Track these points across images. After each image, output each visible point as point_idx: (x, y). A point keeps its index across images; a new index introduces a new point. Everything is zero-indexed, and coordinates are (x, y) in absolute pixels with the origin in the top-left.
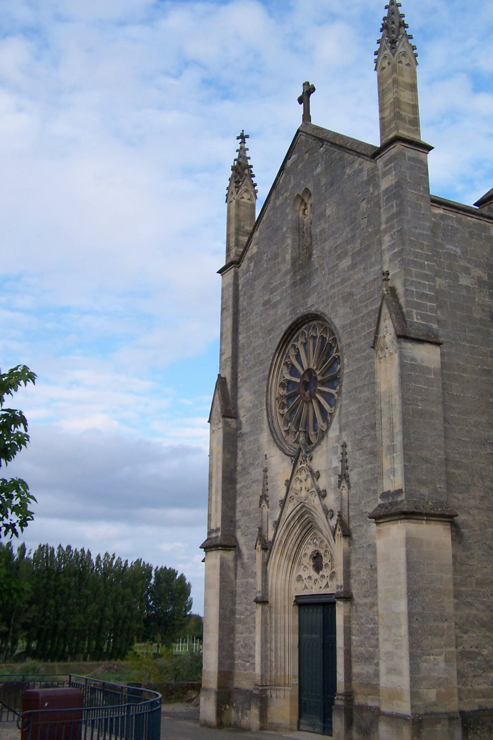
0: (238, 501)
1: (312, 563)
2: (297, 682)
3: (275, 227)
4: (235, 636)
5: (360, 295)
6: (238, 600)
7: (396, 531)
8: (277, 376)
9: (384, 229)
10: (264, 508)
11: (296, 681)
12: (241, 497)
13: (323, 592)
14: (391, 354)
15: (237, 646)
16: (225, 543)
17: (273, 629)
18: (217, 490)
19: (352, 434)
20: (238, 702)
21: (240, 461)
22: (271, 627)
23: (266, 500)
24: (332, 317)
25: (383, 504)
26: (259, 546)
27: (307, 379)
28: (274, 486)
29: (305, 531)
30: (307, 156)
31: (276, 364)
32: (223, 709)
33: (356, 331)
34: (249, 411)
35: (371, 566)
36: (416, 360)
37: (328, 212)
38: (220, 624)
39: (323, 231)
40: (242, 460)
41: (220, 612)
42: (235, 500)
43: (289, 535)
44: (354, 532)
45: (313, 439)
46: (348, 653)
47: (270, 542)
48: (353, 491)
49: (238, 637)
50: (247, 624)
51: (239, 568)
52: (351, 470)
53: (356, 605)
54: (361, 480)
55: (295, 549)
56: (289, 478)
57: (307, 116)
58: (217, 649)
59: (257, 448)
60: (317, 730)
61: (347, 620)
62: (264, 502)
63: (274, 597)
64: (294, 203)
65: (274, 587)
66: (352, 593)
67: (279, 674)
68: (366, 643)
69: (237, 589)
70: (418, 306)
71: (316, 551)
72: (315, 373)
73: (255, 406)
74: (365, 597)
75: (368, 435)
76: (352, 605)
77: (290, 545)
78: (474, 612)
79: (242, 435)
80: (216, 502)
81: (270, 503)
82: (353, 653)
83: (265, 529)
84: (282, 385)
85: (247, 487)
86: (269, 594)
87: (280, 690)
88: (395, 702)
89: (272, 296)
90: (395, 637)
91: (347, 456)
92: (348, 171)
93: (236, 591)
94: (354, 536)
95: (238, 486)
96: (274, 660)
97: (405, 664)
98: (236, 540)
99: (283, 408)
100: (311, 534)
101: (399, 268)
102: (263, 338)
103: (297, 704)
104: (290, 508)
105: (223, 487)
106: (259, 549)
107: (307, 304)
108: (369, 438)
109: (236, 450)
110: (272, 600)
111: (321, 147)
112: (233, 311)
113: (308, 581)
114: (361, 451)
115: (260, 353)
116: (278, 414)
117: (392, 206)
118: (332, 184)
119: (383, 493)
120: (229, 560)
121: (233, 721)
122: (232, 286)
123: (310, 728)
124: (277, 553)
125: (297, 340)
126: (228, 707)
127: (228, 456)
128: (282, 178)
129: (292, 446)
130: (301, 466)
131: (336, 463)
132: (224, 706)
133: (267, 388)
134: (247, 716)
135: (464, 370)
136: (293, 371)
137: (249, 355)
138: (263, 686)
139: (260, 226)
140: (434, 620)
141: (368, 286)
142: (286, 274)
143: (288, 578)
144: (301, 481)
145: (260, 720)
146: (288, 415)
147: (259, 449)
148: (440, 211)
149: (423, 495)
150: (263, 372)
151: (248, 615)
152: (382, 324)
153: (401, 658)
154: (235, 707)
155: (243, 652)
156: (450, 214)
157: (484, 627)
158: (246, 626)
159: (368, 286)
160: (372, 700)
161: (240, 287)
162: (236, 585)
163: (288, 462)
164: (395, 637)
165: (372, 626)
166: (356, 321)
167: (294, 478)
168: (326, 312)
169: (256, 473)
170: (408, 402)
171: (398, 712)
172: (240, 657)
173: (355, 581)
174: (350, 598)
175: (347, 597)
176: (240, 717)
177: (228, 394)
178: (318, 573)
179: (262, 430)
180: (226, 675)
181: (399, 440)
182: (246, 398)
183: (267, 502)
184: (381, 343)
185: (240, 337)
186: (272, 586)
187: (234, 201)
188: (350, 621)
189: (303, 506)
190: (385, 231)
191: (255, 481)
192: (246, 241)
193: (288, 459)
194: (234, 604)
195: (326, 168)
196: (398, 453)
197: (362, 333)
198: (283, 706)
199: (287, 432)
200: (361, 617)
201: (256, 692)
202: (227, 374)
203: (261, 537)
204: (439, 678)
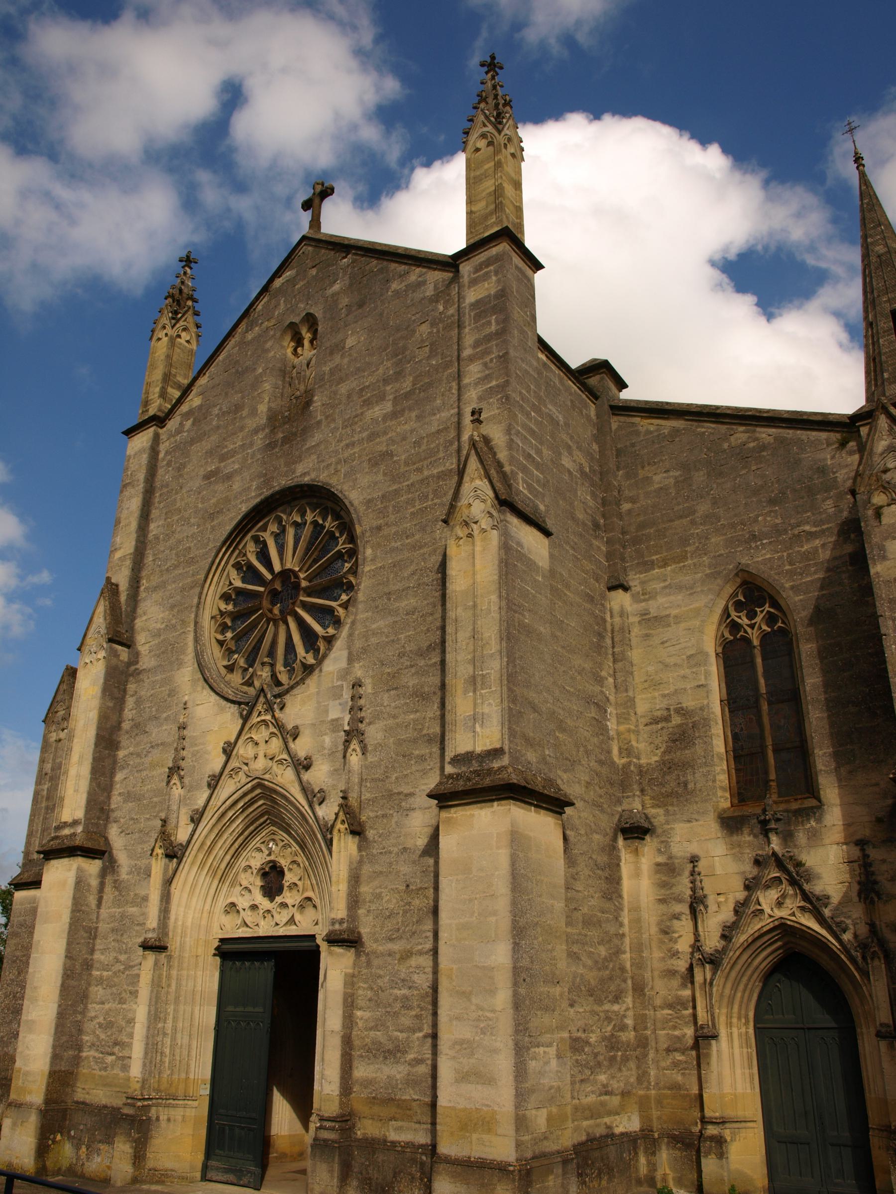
0: (119, 777)
1: (259, 882)
2: (208, 1092)
3: (240, 369)
4: (86, 1007)
5: (407, 455)
6: (99, 944)
7: (490, 821)
8: (218, 583)
9: (470, 356)
10: (174, 787)
11: (206, 1091)
12: (125, 771)
13: (281, 931)
14: (484, 531)
15: (89, 1026)
16: (89, 845)
17: (172, 997)
18: (81, 757)
19: (375, 664)
20: (82, 1127)
21: (128, 713)
22: (168, 993)
23: (179, 775)
24: (345, 487)
25: (458, 775)
26: (159, 851)
27: (278, 586)
28: (198, 752)
29: (252, 828)
30: (314, 272)
31: (219, 564)
32: (50, 1142)
33: (394, 507)
34: (158, 634)
35: (408, 886)
36: (522, 547)
37: (350, 342)
38: (62, 985)
39: (332, 372)
40: (134, 712)
41: (65, 964)
42: (112, 774)
43: (219, 835)
44: (371, 828)
45: (283, 678)
46: (347, 1042)
47: (181, 844)
48: (371, 758)
49: (94, 1009)
50: (115, 986)
51: (108, 889)
52: (370, 724)
53: (368, 954)
54: (391, 740)
55: (228, 857)
56: (232, 741)
57: (316, 223)
58: (53, 1031)
59: (167, 692)
60: (245, 1180)
61: (350, 981)
62: (175, 777)
63: (178, 939)
64: (282, 335)
65: (180, 923)
66: (359, 933)
67: (175, 1077)
68: (389, 1024)
69: (100, 925)
70: (524, 469)
71: (270, 861)
72: (297, 577)
73: (170, 627)
74: (391, 940)
75: (412, 666)
76: (358, 955)
77: (219, 851)
78: (581, 970)
79: (138, 673)
80: (78, 776)
81: (186, 780)
82: (357, 1043)
83: (172, 821)
84: (226, 597)
85: (139, 755)
86: (171, 934)
87: (175, 1106)
88: (475, 1136)
89: (222, 464)
90: (480, 1013)
91: (362, 702)
92: (395, 286)
93: (97, 928)
94: (370, 834)
95: (121, 754)
96: (168, 1053)
97: (503, 1064)
98: (106, 839)
99: (223, 632)
100: (264, 834)
101: (498, 408)
102: (199, 526)
103: (203, 1132)
104: (228, 788)
105: (95, 752)
106: (160, 856)
107: (294, 472)
108: (413, 670)
109: (124, 697)
110: (174, 944)
111: (345, 257)
112: (144, 487)
113: (249, 913)
114: (392, 692)
115: (190, 548)
116: (213, 641)
117: (489, 323)
118: (361, 305)
119: (456, 756)
120: (90, 875)
121: (65, 1164)
122: (148, 451)
123: (231, 1177)
124: (193, 863)
125: (264, 529)
126: (59, 1137)
127: (111, 704)
128: (263, 303)
129: (237, 690)
130: (259, 719)
131: (338, 712)
132: (52, 1137)
133: (200, 598)
134: (98, 1155)
135: (568, 586)
136: (249, 573)
137: (167, 552)
138: (144, 1099)
139: (212, 369)
140: (544, 982)
141: (425, 440)
142: (256, 431)
143: (207, 907)
144: (257, 744)
145: (134, 1164)
146: (233, 642)
147: (172, 693)
148: (542, 357)
149: (529, 763)
150: (193, 575)
151: (119, 971)
152: (467, 487)
153: (496, 1051)
154: (74, 1137)
155: (103, 1036)
156: (553, 367)
157: (591, 995)
158: (114, 990)
159: (425, 440)
160: (398, 1129)
161: (161, 455)
162: (97, 918)
163: (233, 714)
164: (480, 1013)
165: (404, 991)
166: (397, 492)
167: (243, 738)
168: (333, 481)
169: (164, 732)
170: (514, 607)
171: (484, 1156)
172: (93, 1045)
173: (369, 911)
174: (356, 942)
175: (347, 939)
176: (83, 1156)
177: (120, 608)
178: (272, 900)
179: (181, 664)
180: (61, 1078)
181: (494, 668)
182: (151, 616)
183: (181, 778)
184: (463, 513)
185: (152, 526)
186: (176, 919)
187: (165, 339)
188: (353, 984)
189: (259, 785)
190: (471, 359)
191: (158, 745)
192: (177, 397)
193: (234, 708)
194: (92, 951)
195: (351, 285)
196: (493, 689)
197: (406, 509)
198: (180, 1138)
199: (230, 669)
200: (380, 977)
201: (127, 1111)
202: (122, 578)
203: (165, 836)
204: (551, 1088)
